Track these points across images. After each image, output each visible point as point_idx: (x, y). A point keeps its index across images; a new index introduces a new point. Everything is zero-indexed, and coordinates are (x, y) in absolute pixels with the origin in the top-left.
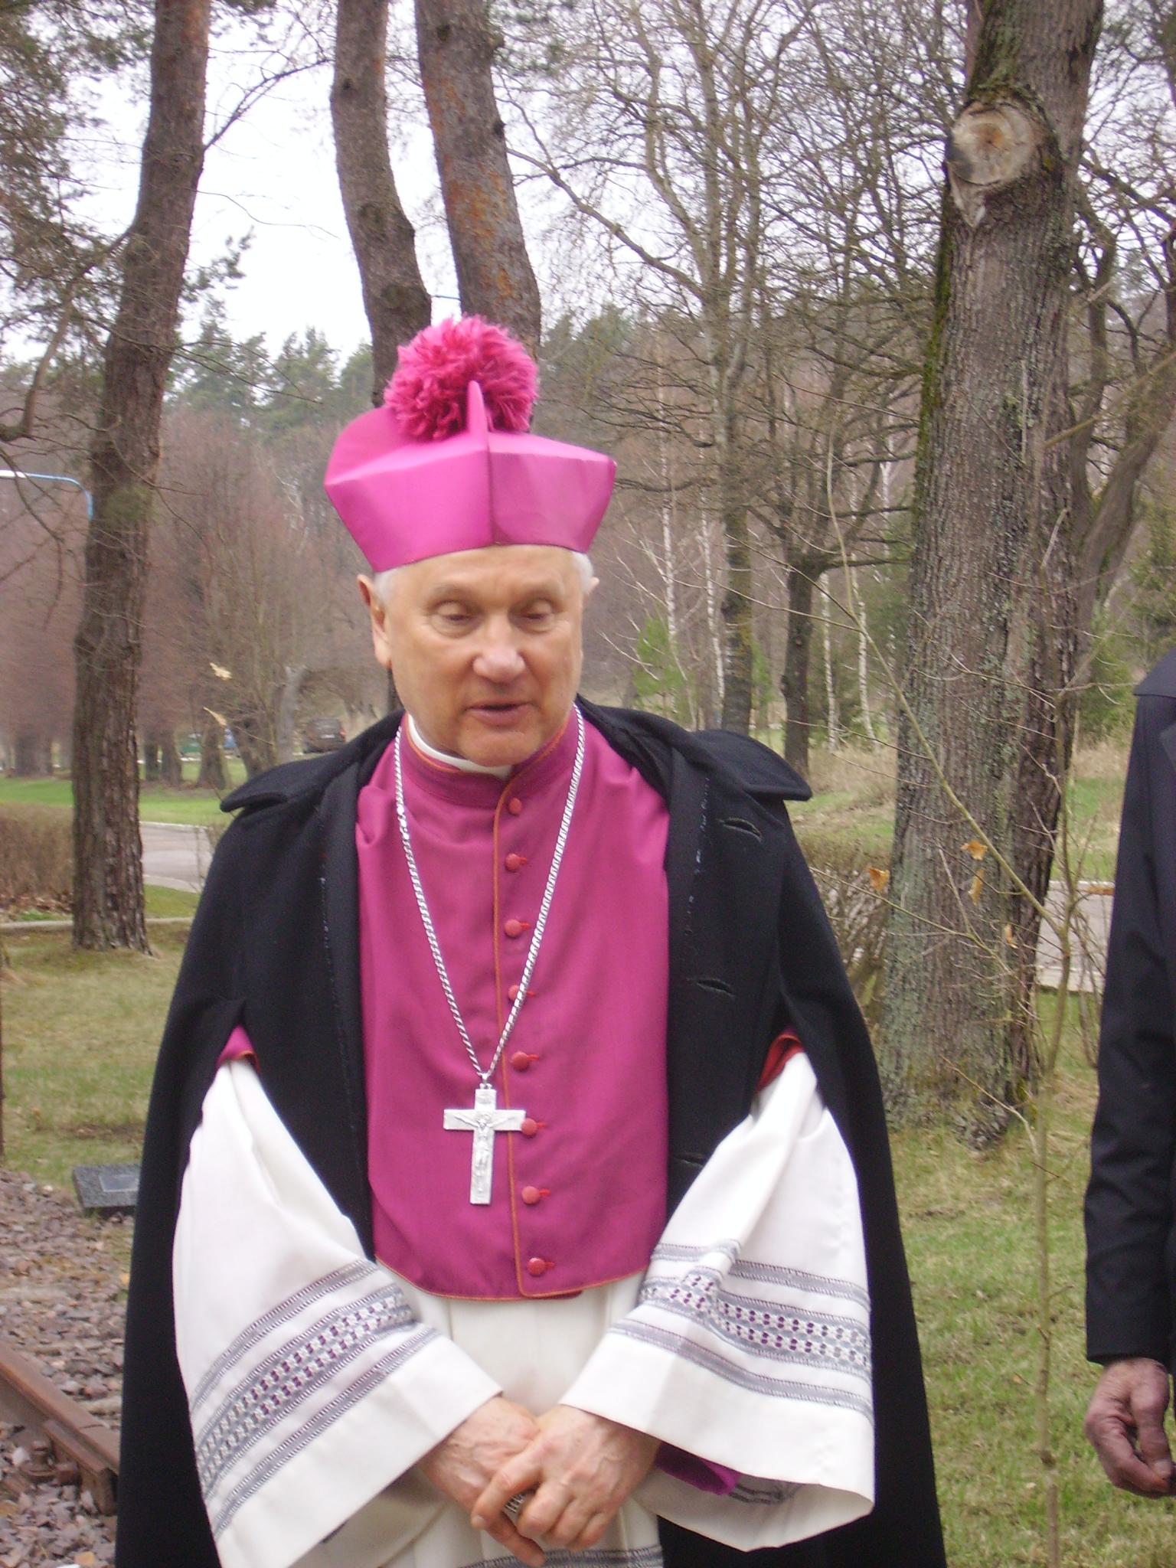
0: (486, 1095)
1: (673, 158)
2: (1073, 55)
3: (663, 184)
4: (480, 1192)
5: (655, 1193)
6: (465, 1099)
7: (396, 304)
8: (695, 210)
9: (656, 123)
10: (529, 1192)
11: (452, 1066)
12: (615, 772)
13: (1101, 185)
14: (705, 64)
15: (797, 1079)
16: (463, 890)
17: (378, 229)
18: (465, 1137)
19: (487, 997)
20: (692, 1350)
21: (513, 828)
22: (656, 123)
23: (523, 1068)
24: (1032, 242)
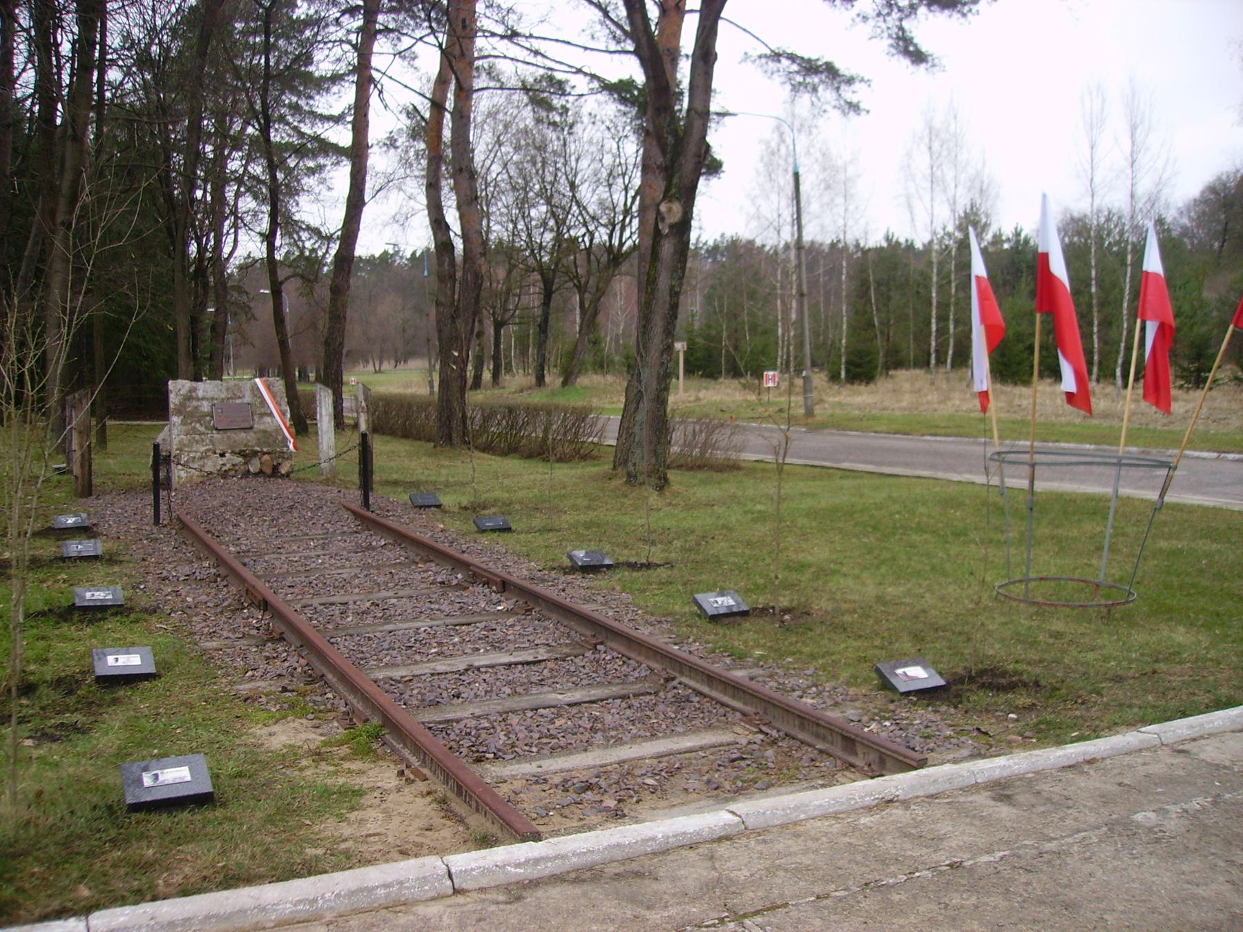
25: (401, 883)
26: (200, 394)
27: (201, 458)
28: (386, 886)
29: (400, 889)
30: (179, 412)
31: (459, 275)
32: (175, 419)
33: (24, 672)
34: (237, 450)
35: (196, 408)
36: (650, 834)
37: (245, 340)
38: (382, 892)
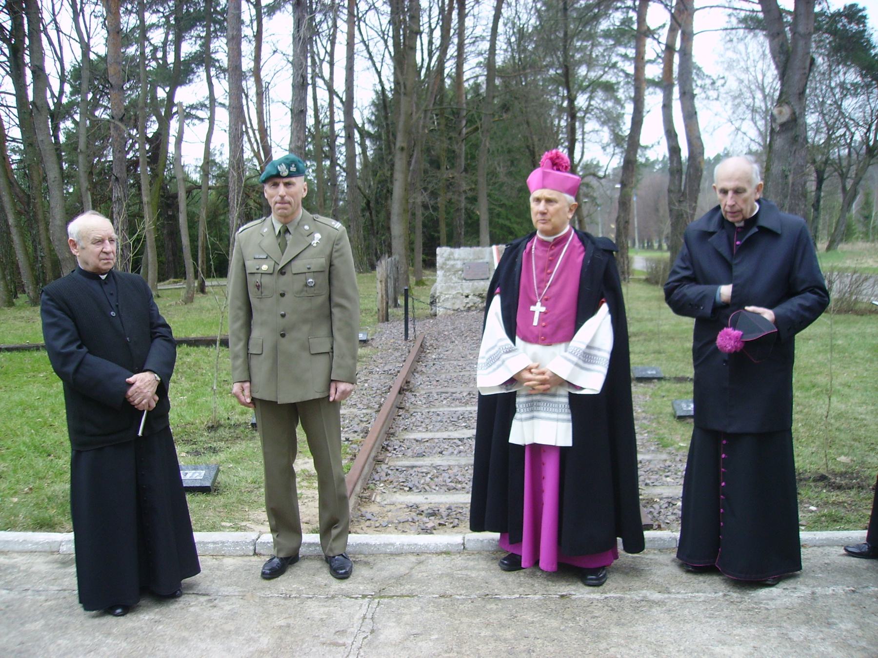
0: (539, 304)
1: (758, 117)
2: (800, 94)
3: (755, 123)
4: (535, 323)
5: (572, 327)
6: (534, 304)
7: (674, 150)
8: (762, 129)
9: (754, 110)
10: (544, 324)
11: (533, 297)
12: (578, 244)
13: (852, 122)
14: (765, 97)
15: (604, 308)
16: (541, 264)
17: (671, 134)
18: (534, 312)
19: (542, 285)
20: (577, 365)
21: (551, 252)
22: (754, 110)
23: (547, 300)
24: (790, 134)
25: (223, 543)
26: (456, 256)
27: (453, 298)
28: (214, 543)
29: (223, 546)
30: (442, 268)
31: (685, 169)
32: (439, 273)
33: (863, 462)
34: (477, 293)
35: (453, 266)
36: (392, 541)
37: (859, 221)
38: (211, 546)
